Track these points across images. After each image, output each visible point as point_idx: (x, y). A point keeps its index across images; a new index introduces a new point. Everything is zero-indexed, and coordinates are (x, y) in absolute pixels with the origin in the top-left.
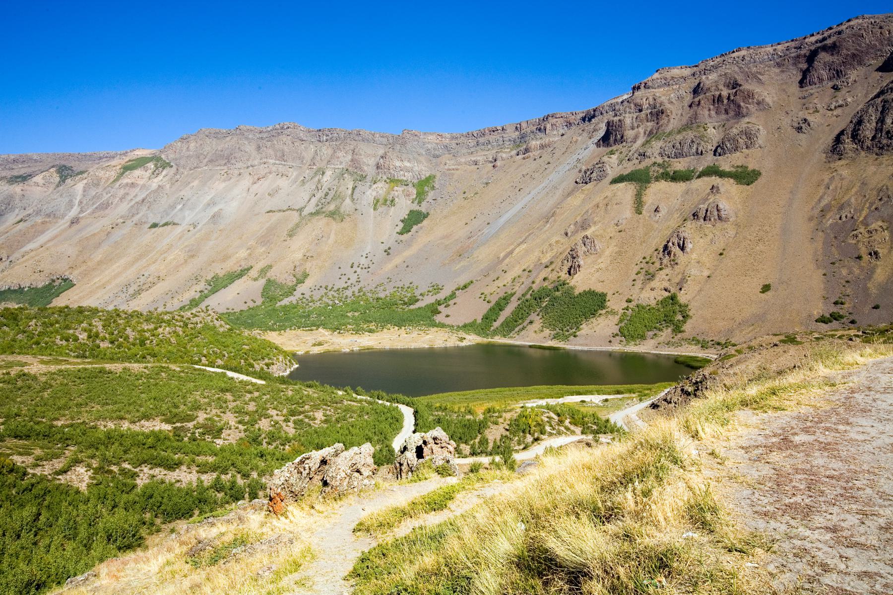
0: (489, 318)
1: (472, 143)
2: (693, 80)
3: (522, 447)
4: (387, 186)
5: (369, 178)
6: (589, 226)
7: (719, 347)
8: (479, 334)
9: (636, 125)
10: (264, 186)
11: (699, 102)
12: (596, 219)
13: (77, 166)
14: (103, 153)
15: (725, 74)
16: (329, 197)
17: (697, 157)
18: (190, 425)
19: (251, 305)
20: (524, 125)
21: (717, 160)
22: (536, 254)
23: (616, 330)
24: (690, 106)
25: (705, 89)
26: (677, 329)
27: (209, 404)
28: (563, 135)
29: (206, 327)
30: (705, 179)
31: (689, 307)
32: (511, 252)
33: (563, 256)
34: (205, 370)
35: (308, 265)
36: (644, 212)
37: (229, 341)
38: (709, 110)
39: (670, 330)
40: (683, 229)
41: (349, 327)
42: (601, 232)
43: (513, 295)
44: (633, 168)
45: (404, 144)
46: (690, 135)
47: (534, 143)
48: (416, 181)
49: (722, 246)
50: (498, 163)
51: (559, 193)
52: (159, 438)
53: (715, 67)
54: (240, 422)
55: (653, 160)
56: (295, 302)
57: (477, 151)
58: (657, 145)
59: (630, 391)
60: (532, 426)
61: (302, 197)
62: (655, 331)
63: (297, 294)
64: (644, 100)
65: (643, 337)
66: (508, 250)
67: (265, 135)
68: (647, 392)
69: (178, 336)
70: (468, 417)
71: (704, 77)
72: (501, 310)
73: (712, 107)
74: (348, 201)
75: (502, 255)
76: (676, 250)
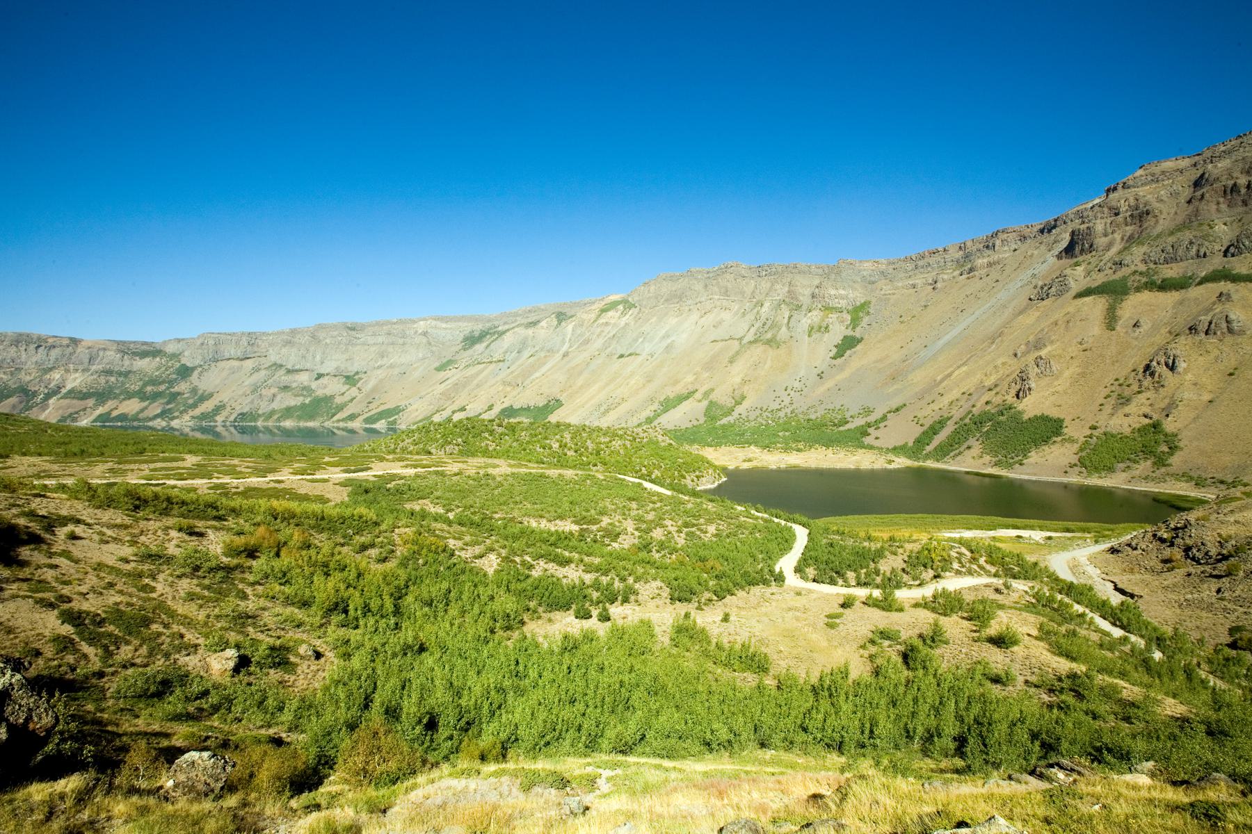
0: (921, 442)
1: (910, 266)
2: (1194, 170)
3: (918, 582)
4: (822, 314)
5: (804, 307)
6: (1045, 346)
7: (1223, 487)
8: (909, 458)
9: (1110, 231)
10: (711, 318)
11: (1203, 196)
12: (1053, 338)
13: (569, 312)
14: (587, 300)
15: (1243, 159)
16: (766, 327)
17: (1197, 261)
18: (594, 528)
19: (695, 423)
20: (969, 244)
21: (1228, 262)
22: (978, 376)
23: (1074, 459)
24: (1189, 202)
25: (1211, 179)
26: (1160, 462)
27: (615, 511)
28: (1015, 250)
29: (651, 442)
30: (1210, 285)
31: (1179, 437)
32: (949, 375)
33: (1011, 378)
34: (624, 480)
35: (746, 388)
36: (1118, 328)
37: (668, 454)
38: (1218, 203)
39: (1149, 463)
40: (1174, 345)
41: (779, 445)
42: (1061, 351)
43: (949, 419)
44: (1105, 280)
45: (839, 273)
46: (1187, 235)
47: (980, 262)
48: (850, 308)
49: (1233, 363)
50: (939, 285)
51: (1008, 313)
52: (561, 539)
53: (1228, 153)
54: (637, 529)
55: (1133, 268)
56: (732, 422)
57: (915, 275)
58: (1138, 251)
59: (1083, 530)
60: (936, 561)
61: (741, 327)
62: (1128, 463)
63: (735, 414)
64: (1122, 202)
65: (1111, 469)
66: (946, 373)
67: (711, 275)
68: (1107, 533)
69: (626, 448)
70: (866, 544)
71: (1210, 166)
72: (935, 434)
73: (1222, 200)
74: (784, 329)
75: (939, 378)
76: (1163, 370)
